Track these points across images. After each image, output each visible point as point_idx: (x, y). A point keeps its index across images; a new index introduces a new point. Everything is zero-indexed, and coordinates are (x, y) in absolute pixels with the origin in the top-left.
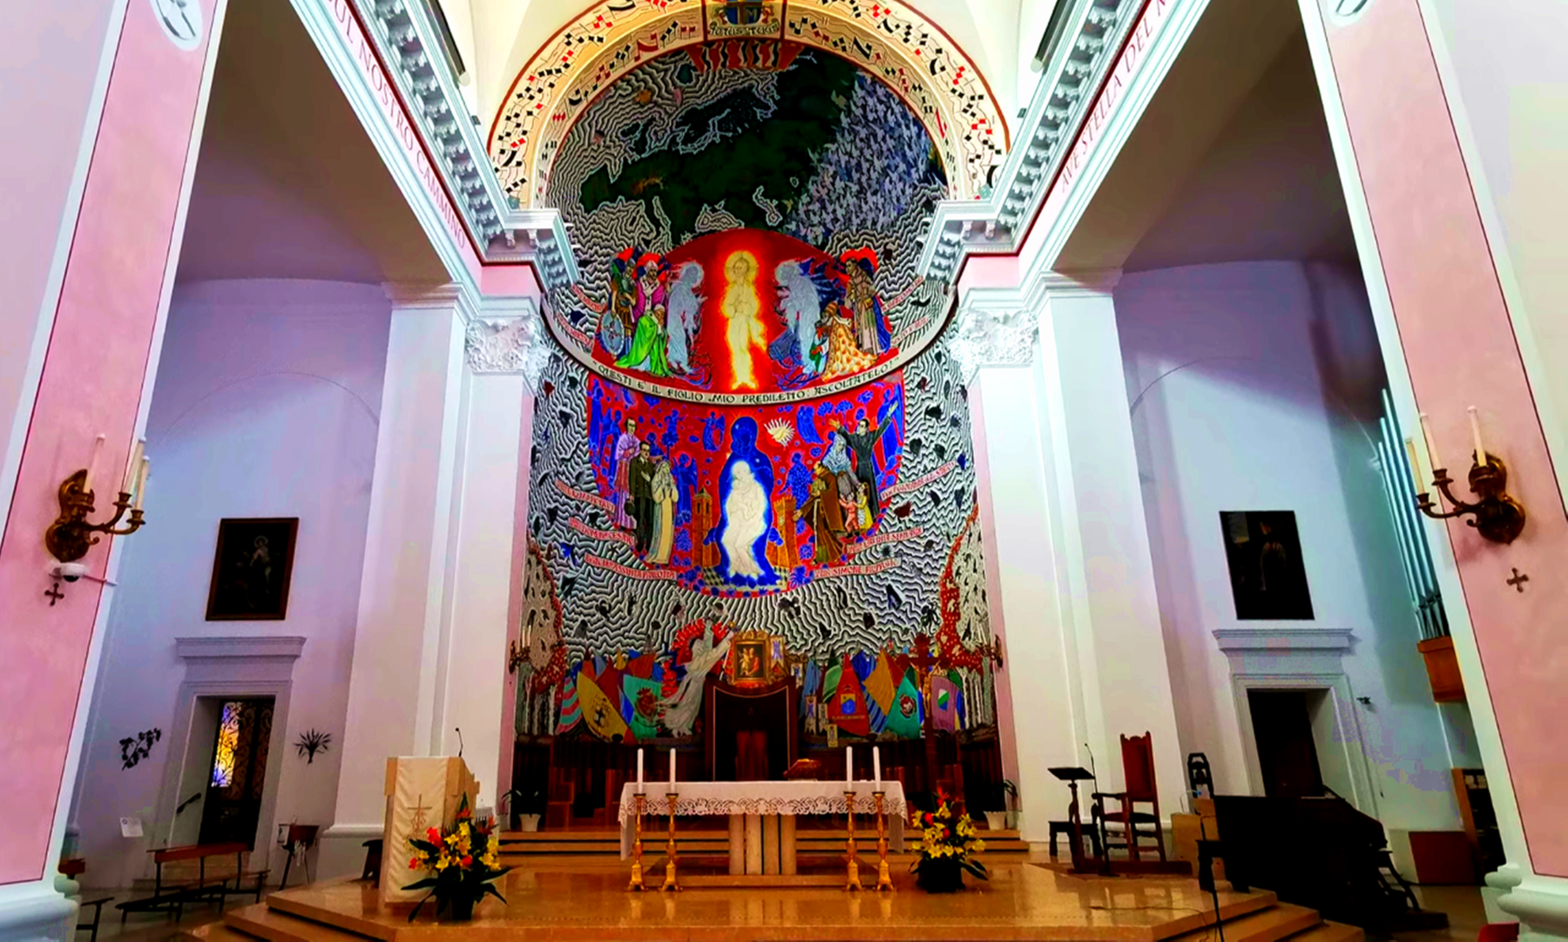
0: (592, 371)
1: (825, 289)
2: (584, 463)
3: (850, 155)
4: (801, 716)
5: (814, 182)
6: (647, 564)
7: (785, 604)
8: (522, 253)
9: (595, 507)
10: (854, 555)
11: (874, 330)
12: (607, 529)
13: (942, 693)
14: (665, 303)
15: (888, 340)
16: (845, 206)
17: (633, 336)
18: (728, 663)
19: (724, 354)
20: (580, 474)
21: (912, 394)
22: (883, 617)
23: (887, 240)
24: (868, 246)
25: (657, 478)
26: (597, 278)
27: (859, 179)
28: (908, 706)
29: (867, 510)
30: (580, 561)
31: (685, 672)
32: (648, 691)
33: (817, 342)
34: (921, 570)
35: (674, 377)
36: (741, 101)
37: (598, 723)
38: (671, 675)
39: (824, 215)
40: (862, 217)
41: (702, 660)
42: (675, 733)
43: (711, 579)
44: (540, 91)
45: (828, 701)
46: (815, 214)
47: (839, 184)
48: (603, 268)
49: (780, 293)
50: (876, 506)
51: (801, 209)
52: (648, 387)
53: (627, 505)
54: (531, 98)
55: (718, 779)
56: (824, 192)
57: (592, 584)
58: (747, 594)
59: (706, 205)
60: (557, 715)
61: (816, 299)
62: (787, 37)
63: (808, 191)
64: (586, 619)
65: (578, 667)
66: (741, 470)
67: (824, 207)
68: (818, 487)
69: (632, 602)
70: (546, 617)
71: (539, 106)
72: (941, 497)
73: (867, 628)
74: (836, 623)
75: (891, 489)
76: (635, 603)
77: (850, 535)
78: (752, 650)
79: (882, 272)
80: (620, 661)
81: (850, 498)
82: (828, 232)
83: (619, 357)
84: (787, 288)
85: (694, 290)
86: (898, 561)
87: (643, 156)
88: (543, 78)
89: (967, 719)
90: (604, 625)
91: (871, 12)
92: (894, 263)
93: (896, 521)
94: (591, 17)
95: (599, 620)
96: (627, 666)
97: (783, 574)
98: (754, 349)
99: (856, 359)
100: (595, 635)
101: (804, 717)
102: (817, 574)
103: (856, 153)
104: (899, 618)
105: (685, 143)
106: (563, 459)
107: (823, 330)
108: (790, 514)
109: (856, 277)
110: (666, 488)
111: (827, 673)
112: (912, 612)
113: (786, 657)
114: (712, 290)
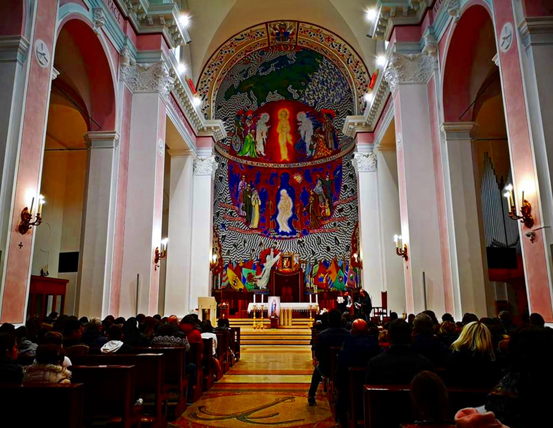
0: (229, 160)
1: (316, 123)
2: (228, 194)
3: (324, 77)
4: (305, 282)
5: (311, 84)
6: (250, 229)
7: (299, 242)
8: (209, 133)
9: (232, 209)
10: (324, 225)
11: (332, 141)
12: (236, 216)
13: (351, 275)
14: (255, 129)
15: (338, 147)
16: (322, 93)
17: (243, 143)
18: (279, 263)
19: (278, 148)
20: (227, 198)
21: (345, 168)
22: (333, 248)
23: (337, 108)
24: (331, 109)
25: (253, 197)
26: (231, 123)
27: (327, 85)
28: (341, 279)
29: (329, 208)
30: (227, 229)
31: (264, 267)
32: (251, 273)
33: (312, 143)
34: (346, 232)
35: (259, 158)
36: (283, 60)
37: (234, 285)
38: (259, 268)
39: (315, 96)
40: (329, 98)
41: (270, 262)
42: (260, 288)
43: (273, 233)
44: (212, 72)
45: (314, 277)
46: (311, 95)
47: (320, 85)
48: (232, 119)
49: (298, 124)
50: (332, 208)
51: (306, 93)
52: (249, 163)
53: (242, 208)
54: (210, 74)
55: (301, 302)
56: (314, 88)
57: (231, 237)
58: (286, 239)
59: (270, 92)
60: (221, 283)
61: (312, 127)
62: (298, 45)
63: (308, 87)
64: (230, 249)
65: (227, 266)
66: (284, 192)
67: (314, 93)
68: (312, 199)
69: (245, 242)
70: (217, 250)
71: (212, 78)
72: (353, 207)
73: (328, 251)
74: (317, 249)
75: (337, 202)
76: (246, 242)
77: (322, 218)
78: (287, 259)
79: (336, 119)
80: (241, 263)
81: (323, 204)
82: (316, 102)
83: (239, 152)
84: (301, 122)
85: (266, 123)
86: (338, 228)
87: (247, 78)
88: (213, 67)
89: (358, 284)
90: (236, 251)
91: (327, 40)
92: (340, 117)
93: (338, 214)
94: (229, 43)
95: (234, 249)
96: (244, 265)
97: (299, 231)
98: (288, 145)
99: (326, 151)
100: (232, 254)
101: (306, 282)
102: (311, 232)
103: (325, 77)
104: (338, 249)
105: (262, 72)
106: (221, 194)
107: (314, 139)
108: (301, 209)
109: (327, 120)
110: (257, 200)
111: (314, 267)
112: (343, 247)
113: (300, 261)
114: (272, 124)
